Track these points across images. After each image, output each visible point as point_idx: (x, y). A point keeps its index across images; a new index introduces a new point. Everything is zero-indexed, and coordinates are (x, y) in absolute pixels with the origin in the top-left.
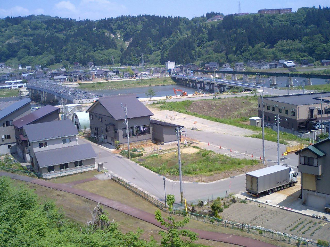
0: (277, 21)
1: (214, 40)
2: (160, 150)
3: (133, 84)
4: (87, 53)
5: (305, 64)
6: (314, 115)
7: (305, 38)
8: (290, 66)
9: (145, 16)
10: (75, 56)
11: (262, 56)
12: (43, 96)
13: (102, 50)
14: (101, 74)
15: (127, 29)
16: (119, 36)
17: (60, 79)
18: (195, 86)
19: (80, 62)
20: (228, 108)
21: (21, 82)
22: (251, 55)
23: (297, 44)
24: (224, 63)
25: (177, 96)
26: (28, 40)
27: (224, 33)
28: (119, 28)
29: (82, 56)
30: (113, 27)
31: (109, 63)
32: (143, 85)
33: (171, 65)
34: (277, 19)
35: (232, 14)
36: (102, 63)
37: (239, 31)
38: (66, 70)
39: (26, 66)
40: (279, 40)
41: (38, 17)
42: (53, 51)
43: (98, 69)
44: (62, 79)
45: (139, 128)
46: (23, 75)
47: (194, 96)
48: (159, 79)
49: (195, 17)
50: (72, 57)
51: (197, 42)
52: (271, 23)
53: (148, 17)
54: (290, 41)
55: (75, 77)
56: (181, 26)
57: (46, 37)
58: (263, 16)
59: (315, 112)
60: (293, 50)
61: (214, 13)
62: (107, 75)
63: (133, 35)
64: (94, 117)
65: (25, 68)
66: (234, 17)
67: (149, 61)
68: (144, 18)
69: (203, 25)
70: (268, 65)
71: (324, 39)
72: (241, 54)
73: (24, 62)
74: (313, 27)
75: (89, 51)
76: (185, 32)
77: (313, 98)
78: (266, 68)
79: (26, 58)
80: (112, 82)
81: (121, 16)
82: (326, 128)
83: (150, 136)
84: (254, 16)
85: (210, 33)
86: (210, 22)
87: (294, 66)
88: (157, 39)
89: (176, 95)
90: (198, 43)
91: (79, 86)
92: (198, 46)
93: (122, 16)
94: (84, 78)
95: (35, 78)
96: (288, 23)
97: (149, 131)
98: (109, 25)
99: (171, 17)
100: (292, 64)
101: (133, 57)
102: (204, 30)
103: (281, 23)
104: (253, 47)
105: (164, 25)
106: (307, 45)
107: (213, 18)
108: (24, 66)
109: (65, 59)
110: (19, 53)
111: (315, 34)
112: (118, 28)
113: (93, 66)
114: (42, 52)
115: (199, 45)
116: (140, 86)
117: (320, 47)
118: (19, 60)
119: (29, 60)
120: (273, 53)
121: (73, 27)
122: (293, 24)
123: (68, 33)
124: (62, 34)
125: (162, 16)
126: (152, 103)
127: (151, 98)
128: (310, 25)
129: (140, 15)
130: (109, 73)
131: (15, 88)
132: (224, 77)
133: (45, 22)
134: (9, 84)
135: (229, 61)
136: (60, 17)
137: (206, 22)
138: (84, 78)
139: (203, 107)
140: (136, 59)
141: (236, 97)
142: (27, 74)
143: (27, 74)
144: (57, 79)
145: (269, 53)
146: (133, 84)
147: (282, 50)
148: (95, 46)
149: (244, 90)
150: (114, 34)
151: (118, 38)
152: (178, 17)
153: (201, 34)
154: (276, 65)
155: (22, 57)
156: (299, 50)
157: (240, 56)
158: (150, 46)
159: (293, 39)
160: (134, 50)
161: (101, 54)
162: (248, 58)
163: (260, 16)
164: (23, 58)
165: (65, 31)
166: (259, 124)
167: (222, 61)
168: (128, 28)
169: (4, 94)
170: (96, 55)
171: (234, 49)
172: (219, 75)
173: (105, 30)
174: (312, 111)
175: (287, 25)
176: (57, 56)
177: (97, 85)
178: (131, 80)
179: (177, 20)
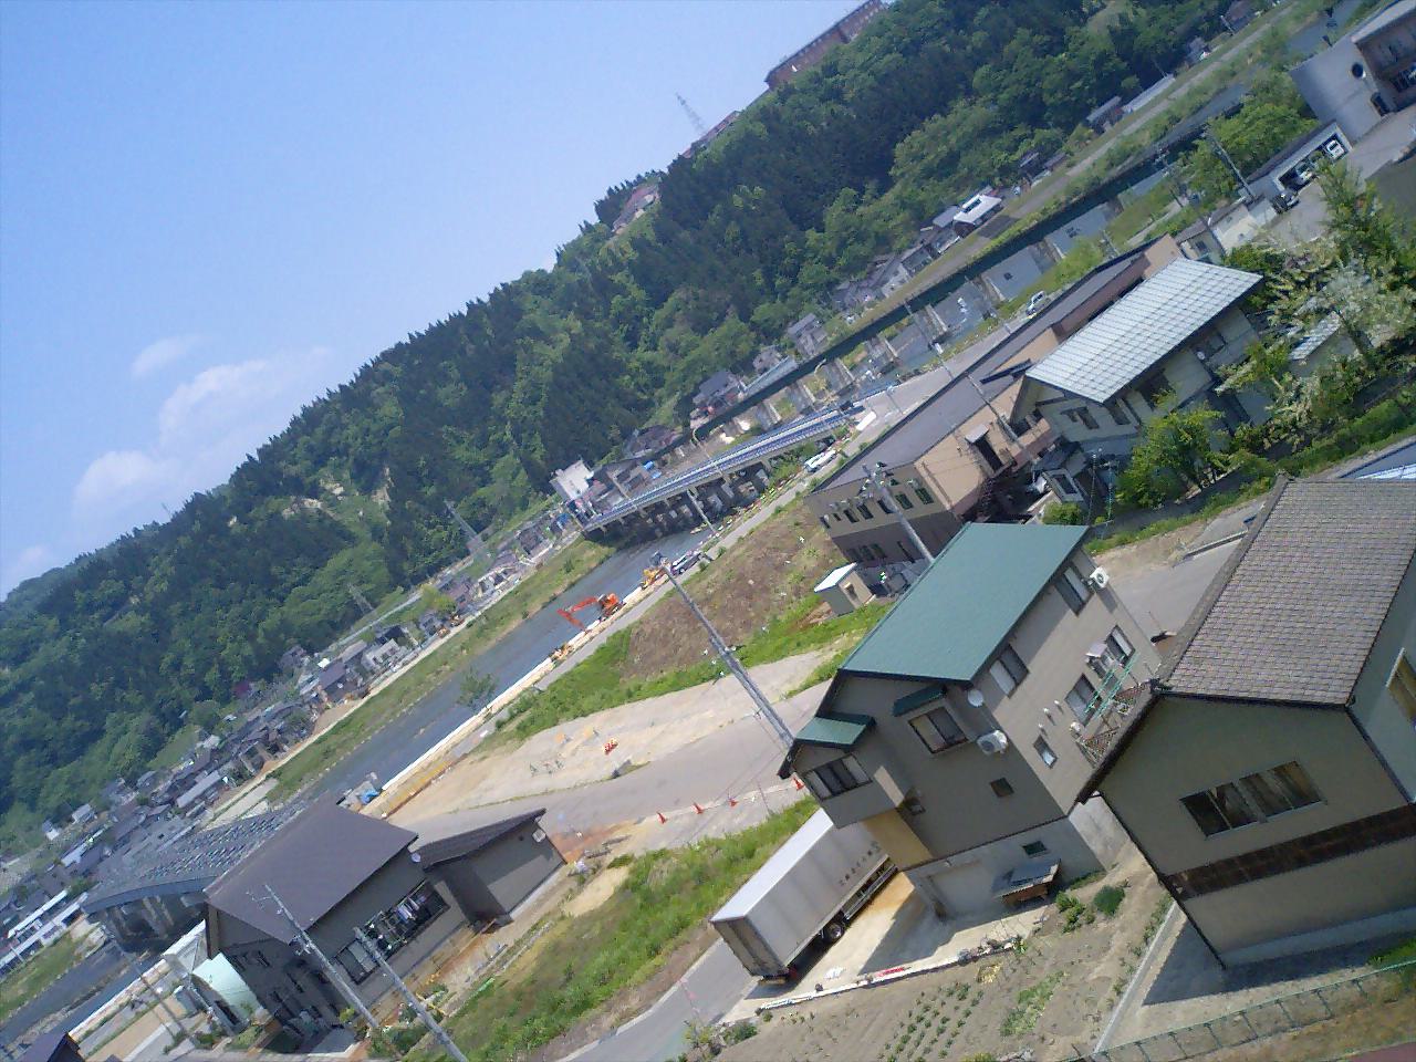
0: (852, 73)
1: (673, 291)
2: (497, 954)
3: (465, 651)
4: (257, 625)
5: (1035, 170)
6: (997, 452)
7: (978, 77)
8: (983, 218)
9: (386, 356)
10: (222, 663)
11: (870, 243)
12: (153, 912)
13: (305, 580)
14: (339, 681)
15: (348, 446)
16: (338, 491)
17: (202, 796)
18: (677, 520)
19: (255, 674)
20: (751, 582)
21: (68, 900)
22: (830, 262)
23: (968, 115)
24: (754, 353)
25: (589, 628)
26: (23, 713)
27: (691, 242)
28: (320, 462)
29: (248, 650)
30: (293, 470)
31: (354, 614)
32: (500, 633)
33: (575, 480)
34: (847, 68)
35: (680, 157)
36: (334, 626)
37: (738, 201)
38: (221, 736)
39: (71, 813)
40: (893, 141)
41: (14, 597)
42: (132, 697)
43: (324, 663)
44: (209, 792)
45: (395, 917)
46: (67, 861)
47: (647, 591)
48: (545, 573)
49: (563, 248)
50: (212, 676)
51: (618, 335)
52: (836, 94)
53: (395, 355)
54: (936, 123)
55: (251, 753)
56: (532, 310)
57: (77, 660)
58: (790, 91)
59: (998, 443)
60: (968, 146)
61: (620, 188)
62: (368, 668)
63: (383, 454)
64: (242, 960)
65: (71, 820)
66: (691, 161)
67: (494, 511)
68: (386, 366)
69: (603, 263)
70: (901, 266)
71: (1047, 38)
72: (795, 282)
73: (53, 802)
74: (988, 17)
75: (261, 617)
76: (560, 324)
77: (984, 382)
78: (902, 282)
79: (54, 785)
80: (384, 693)
81: (299, 413)
82: (1058, 479)
83: (455, 913)
84: (762, 113)
85: (642, 274)
86: (623, 235)
87: (998, 205)
88: (476, 412)
89: (582, 627)
90: (626, 339)
91: (274, 783)
92: (634, 346)
93: (305, 409)
94: (288, 737)
95: (115, 849)
96: (894, 55)
97: (442, 902)
98: (279, 474)
99: (475, 302)
100: (986, 201)
101: (430, 532)
102: (618, 278)
103: (872, 73)
104: (821, 229)
105: (470, 348)
106: (1004, 96)
107: (627, 208)
108: (60, 818)
109: (196, 700)
110: (18, 780)
111: (1007, 41)
112: (315, 463)
113: (307, 659)
114: (95, 726)
115: (632, 340)
116: (493, 642)
117: (1048, 74)
118: (32, 807)
119: (67, 786)
120: (903, 204)
121: (153, 560)
122: (912, 49)
123: (150, 597)
124: (130, 615)
125: (444, 319)
126: (493, 729)
127: (489, 706)
128: (974, 13)
129: (367, 366)
130: (369, 657)
131: (52, 938)
132: (768, 414)
133: (46, 608)
134: (25, 936)
135: (770, 334)
136: (93, 552)
137: (610, 243)
138: (288, 737)
139: (671, 630)
140: (444, 534)
141: (779, 510)
142: (80, 850)
143: (80, 850)
144: (191, 805)
145: (886, 214)
146: (462, 648)
147: (929, 173)
148: (269, 583)
149: (822, 445)
150: (314, 492)
151: (340, 498)
152: (501, 288)
153: (616, 300)
154: (929, 248)
155: (37, 791)
156: (988, 132)
157: (795, 291)
158: (467, 454)
159: (942, 108)
160: (417, 505)
161: (310, 597)
162: (825, 278)
163: (783, 97)
164: (43, 793)
165: (136, 592)
166: (855, 590)
167: (744, 348)
168: (350, 440)
169: (19, 989)
170: (294, 610)
171: (760, 282)
172: (750, 418)
173: (274, 503)
174: (983, 445)
175: (893, 66)
176: (161, 705)
177: (338, 737)
178: (448, 642)
179: (506, 302)
